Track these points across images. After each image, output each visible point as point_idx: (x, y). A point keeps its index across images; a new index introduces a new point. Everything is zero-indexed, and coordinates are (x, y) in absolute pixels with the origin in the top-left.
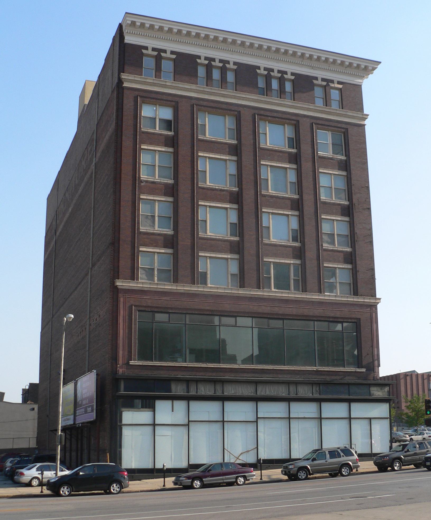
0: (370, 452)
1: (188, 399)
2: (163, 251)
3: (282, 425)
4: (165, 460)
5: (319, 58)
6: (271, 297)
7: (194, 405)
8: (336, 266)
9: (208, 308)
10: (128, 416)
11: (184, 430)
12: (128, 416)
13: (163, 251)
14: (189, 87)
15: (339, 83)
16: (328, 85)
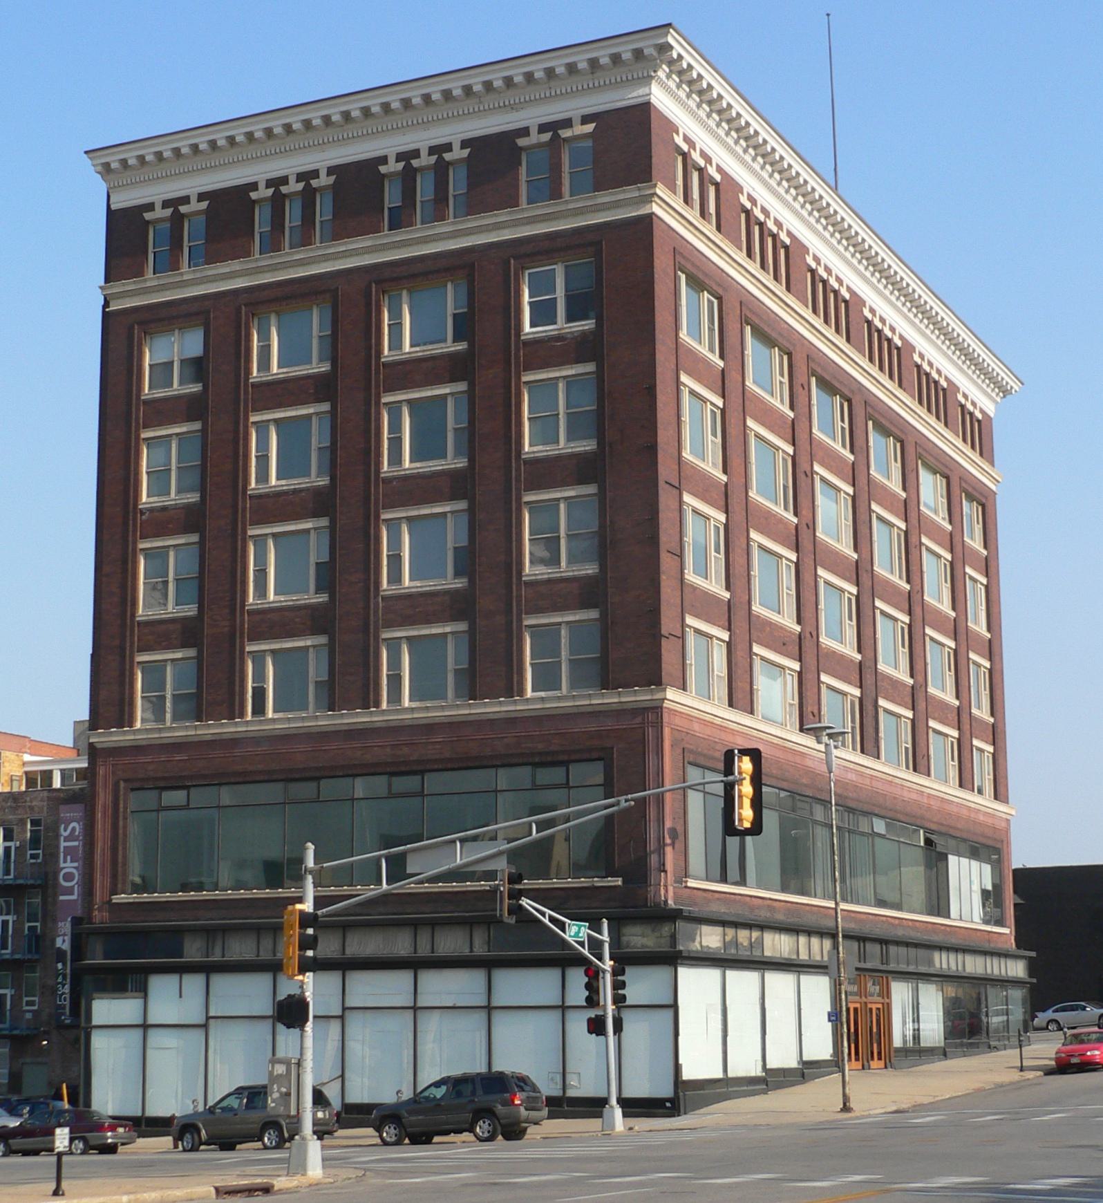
1: (208, 969)
2: (179, 655)
4: (169, 1100)
6: (392, 724)
7: (221, 983)
8: (560, 620)
9: (260, 767)
10: (104, 1009)
11: (199, 1035)
12: (104, 1009)
13: (179, 655)
14: (228, 270)
15: (585, 120)
16: (556, 136)
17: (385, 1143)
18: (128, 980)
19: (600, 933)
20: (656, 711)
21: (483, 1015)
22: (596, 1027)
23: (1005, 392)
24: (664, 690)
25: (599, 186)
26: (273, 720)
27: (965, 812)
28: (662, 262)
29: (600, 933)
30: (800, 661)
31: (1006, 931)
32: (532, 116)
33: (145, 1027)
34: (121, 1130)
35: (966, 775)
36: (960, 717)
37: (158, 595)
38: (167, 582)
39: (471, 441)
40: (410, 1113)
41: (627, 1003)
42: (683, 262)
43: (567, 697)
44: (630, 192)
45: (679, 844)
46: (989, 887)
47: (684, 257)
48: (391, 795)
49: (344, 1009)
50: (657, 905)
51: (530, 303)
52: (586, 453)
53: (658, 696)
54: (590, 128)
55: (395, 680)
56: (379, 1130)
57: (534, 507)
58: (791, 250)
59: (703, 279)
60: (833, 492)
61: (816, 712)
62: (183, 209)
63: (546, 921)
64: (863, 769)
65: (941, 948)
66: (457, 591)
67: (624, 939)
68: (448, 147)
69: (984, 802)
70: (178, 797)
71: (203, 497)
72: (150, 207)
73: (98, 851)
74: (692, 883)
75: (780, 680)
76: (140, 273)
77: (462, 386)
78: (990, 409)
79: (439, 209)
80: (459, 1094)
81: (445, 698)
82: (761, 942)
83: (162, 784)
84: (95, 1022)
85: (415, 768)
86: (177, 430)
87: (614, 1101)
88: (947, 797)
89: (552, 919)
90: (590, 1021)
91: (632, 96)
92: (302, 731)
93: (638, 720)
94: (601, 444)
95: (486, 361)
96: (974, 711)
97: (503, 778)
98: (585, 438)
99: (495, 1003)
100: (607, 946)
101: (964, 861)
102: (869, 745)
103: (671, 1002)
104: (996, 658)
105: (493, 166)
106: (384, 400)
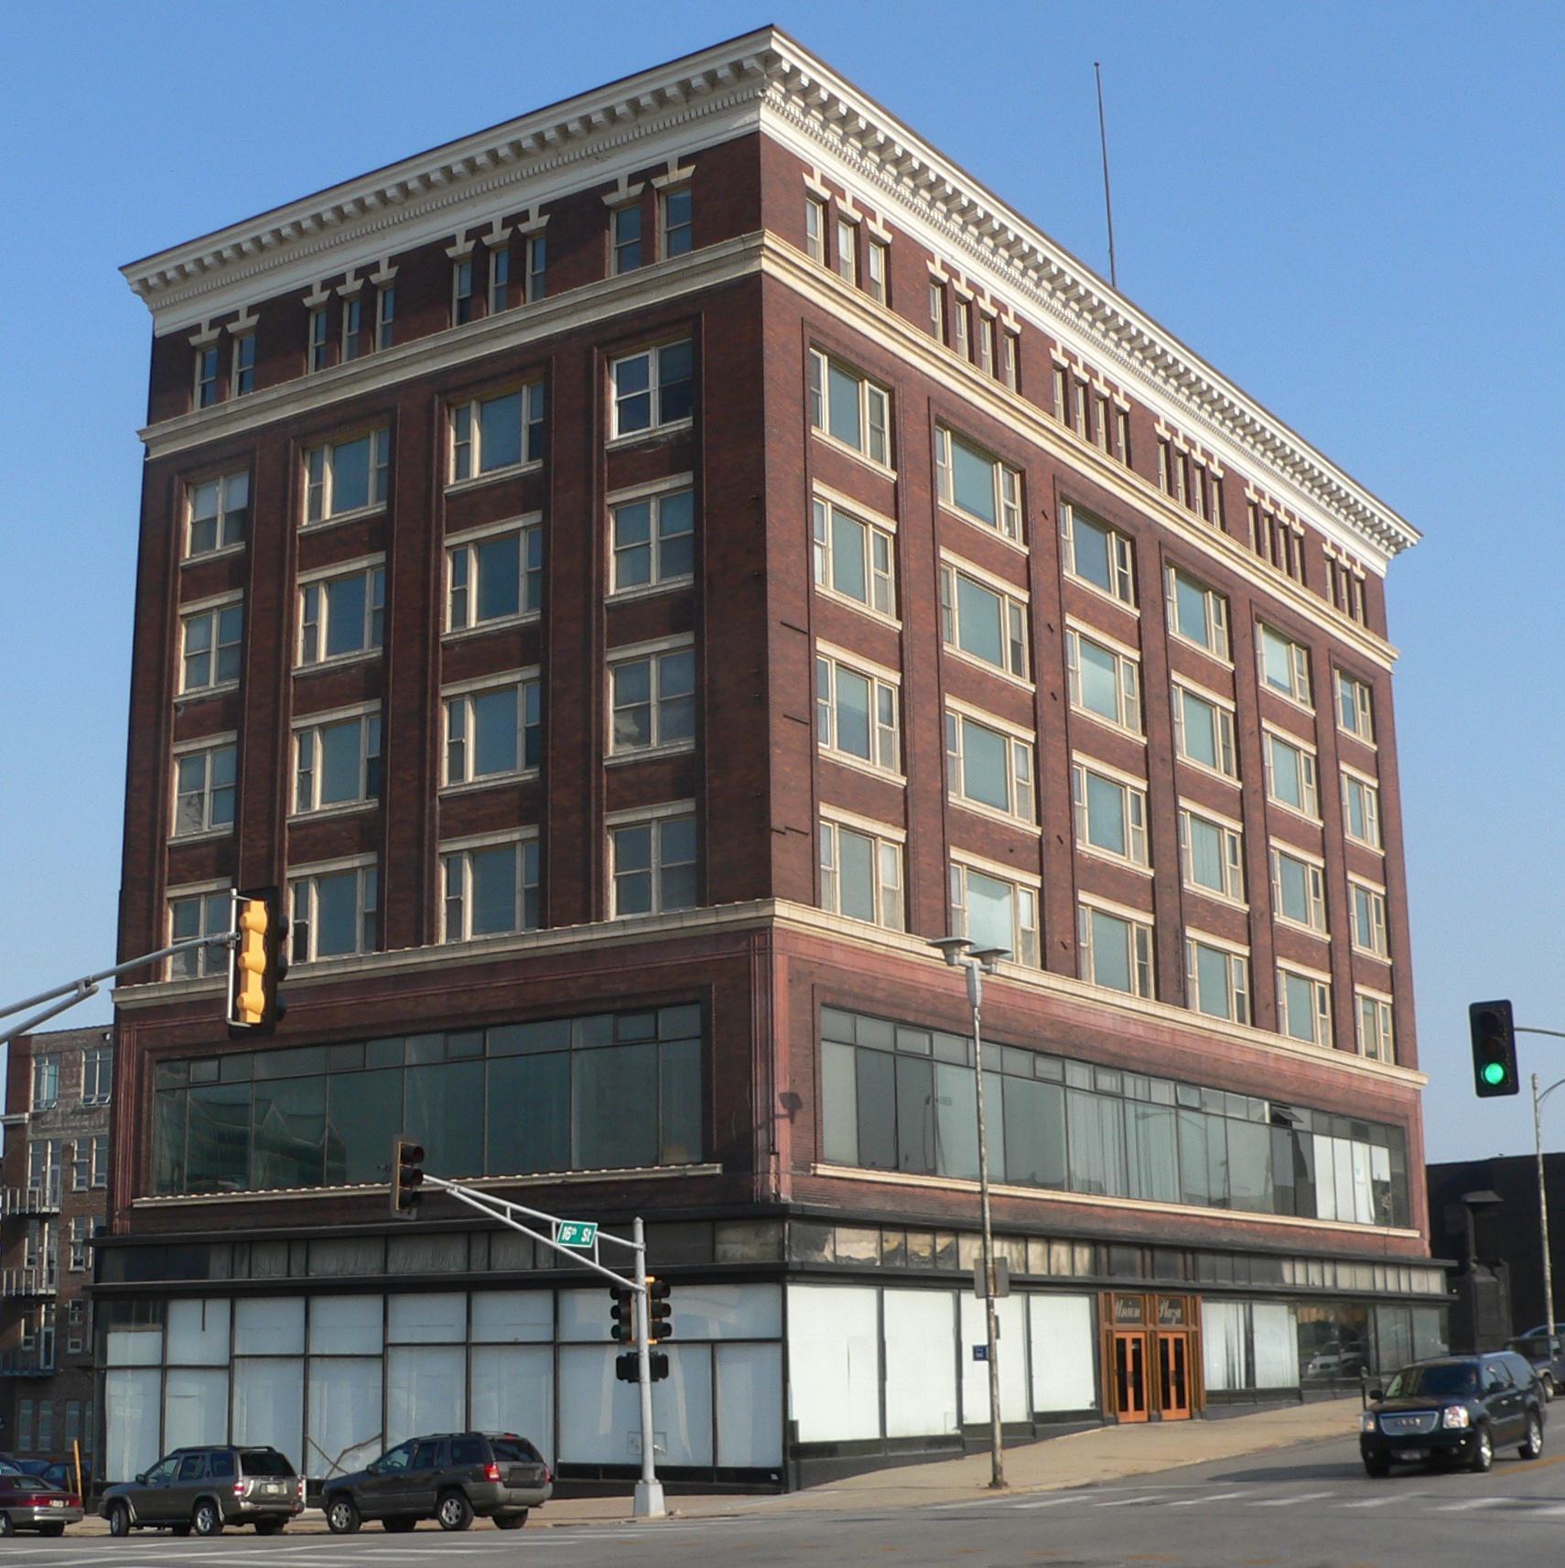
1: (235, 1293)
10: (126, 1346)
11: (222, 1378)
14: (275, 396)
15: (683, 162)
17: (334, 1530)
18: (146, 1309)
19: (633, 1240)
20: (763, 931)
21: (547, 1354)
22: (628, 1369)
23: (1399, 546)
24: (772, 903)
25: (697, 244)
26: (313, 965)
27: (1342, 1080)
28: (777, 335)
29: (633, 1240)
30: (1041, 873)
31: (1415, 1234)
32: (619, 166)
33: (164, 1368)
34: (56, 1504)
35: (1344, 1028)
36: (1335, 956)
37: (192, 811)
38: (201, 795)
39: (545, 587)
40: (365, 1489)
41: (672, 1337)
42: (818, 337)
43: (661, 919)
44: (733, 246)
45: (803, 1116)
46: (1386, 1177)
47: (820, 332)
48: (449, 1061)
49: (386, 1346)
50: (765, 1200)
51: (619, 403)
52: (681, 590)
53: (765, 912)
54: (688, 171)
55: (455, 907)
56: (328, 1511)
57: (620, 668)
58: (1022, 339)
59: (855, 363)
60: (1108, 658)
61: (1069, 941)
62: (232, 328)
63: (508, 1220)
64: (1158, 1021)
65: (1293, 1257)
66: (526, 785)
67: (720, 1248)
68: (524, 216)
69: (1384, 1069)
70: (207, 1070)
71: (242, 684)
72: (196, 329)
73: (120, 1142)
74: (823, 1170)
75: (1007, 900)
76: (183, 410)
77: (535, 517)
78: (1380, 567)
79: (512, 295)
80: (429, 1463)
81: (511, 927)
82: (953, 1252)
83: (190, 1054)
84: (110, 1362)
85: (475, 1022)
86: (218, 602)
87: (650, 1473)
88: (1309, 1059)
89: (516, 1215)
90: (619, 1360)
91: (736, 126)
92: (346, 978)
93: (743, 945)
94: (698, 578)
95: (564, 482)
96: (1358, 948)
97: (579, 1032)
98: (680, 573)
99: (566, 1336)
100: (641, 1257)
101: (1342, 1145)
102: (1169, 988)
103: (778, 1334)
104: (1394, 882)
105: (575, 235)
106: (447, 543)
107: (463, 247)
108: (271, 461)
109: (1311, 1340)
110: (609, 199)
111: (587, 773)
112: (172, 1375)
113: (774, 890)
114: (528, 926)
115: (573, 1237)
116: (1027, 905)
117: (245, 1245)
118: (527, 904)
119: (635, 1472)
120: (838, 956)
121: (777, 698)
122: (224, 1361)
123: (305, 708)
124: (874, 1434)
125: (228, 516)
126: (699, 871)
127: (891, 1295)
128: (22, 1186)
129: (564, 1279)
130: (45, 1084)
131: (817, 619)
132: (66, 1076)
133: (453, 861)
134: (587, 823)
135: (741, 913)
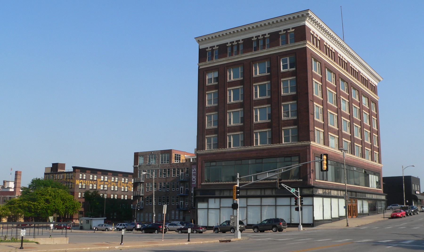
0: (275, 218)
1: (220, 198)
3: (258, 208)
5: (277, 21)
10: (200, 205)
11: (219, 210)
12: (200, 205)
15: (292, 28)
17: (255, 232)
18: (205, 200)
20: (309, 146)
21: (275, 207)
23: (380, 81)
25: (296, 41)
26: (233, 148)
28: (308, 56)
32: (282, 28)
33: (208, 209)
35: (373, 158)
37: (210, 124)
43: (291, 143)
44: (302, 43)
48: (256, 163)
52: (294, 95)
54: (293, 30)
56: (254, 229)
59: (317, 59)
65: (368, 193)
70: (214, 164)
72: (207, 48)
74: (316, 181)
76: (205, 61)
77: (269, 82)
78: (377, 84)
87: (300, 224)
89: (288, 188)
90: (296, 208)
91: (302, 24)
99: (277, 204)
101: (372, 176)
102: (353, 152)
105: (274, 38)
107: (255, 39)
108: (222, 70)
109: (370, 206)
110: (280, 33)
111: (279, 121)
112: (209, 210)
113: (311, 139)
114: (269, 143)
115: (293, 191)
116: (337, 140)
117: (221, 190)
118: (269, 140)
119: (298, 224)
120: (317, 149)
121: (310, 111)
122: (219, 207)
123: (230, 109)
124: (322, 219)
125: (214, 78)
126: (298, 136)
127: (324, 199)
128: (137, 177)
129: (291, 196)
130: (141, 161)
131: (315, 99)
132: (145, 159)
133: (256, 133)
134: (279, 129)
135: (306, 143)
